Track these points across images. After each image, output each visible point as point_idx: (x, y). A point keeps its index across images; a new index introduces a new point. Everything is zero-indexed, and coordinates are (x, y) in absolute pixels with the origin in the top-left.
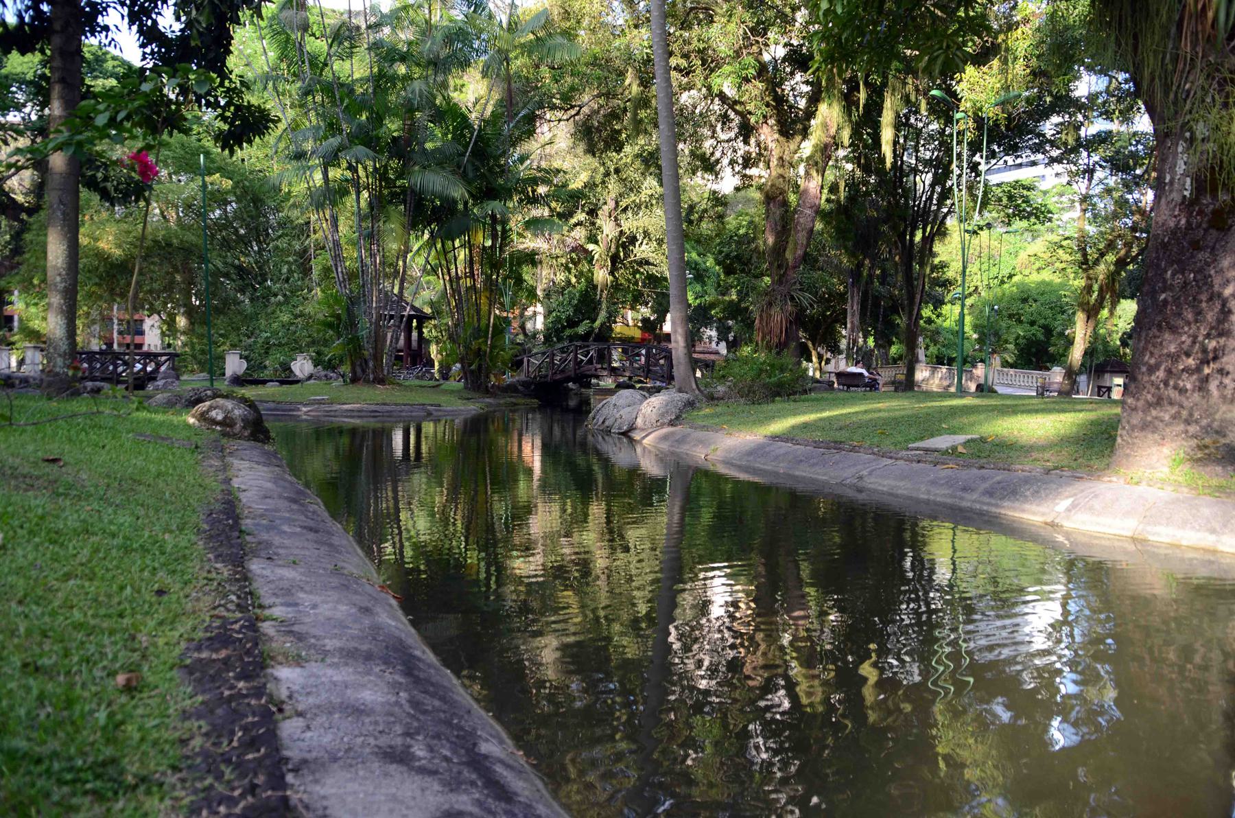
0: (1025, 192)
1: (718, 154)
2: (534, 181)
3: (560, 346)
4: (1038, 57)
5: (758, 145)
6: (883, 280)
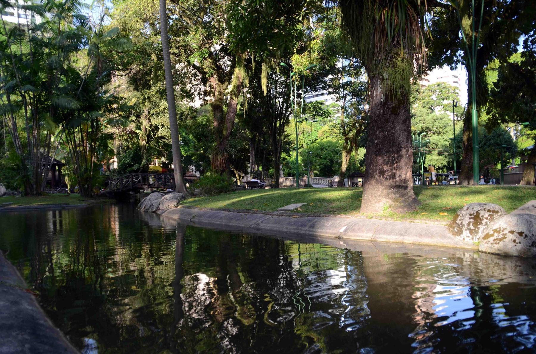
0: (320, 106)
1: (193, 91)
2: (111, 103)
3: (125, 175)
4: (323, 51)
5: (210, 86)
6: (265, 142)
